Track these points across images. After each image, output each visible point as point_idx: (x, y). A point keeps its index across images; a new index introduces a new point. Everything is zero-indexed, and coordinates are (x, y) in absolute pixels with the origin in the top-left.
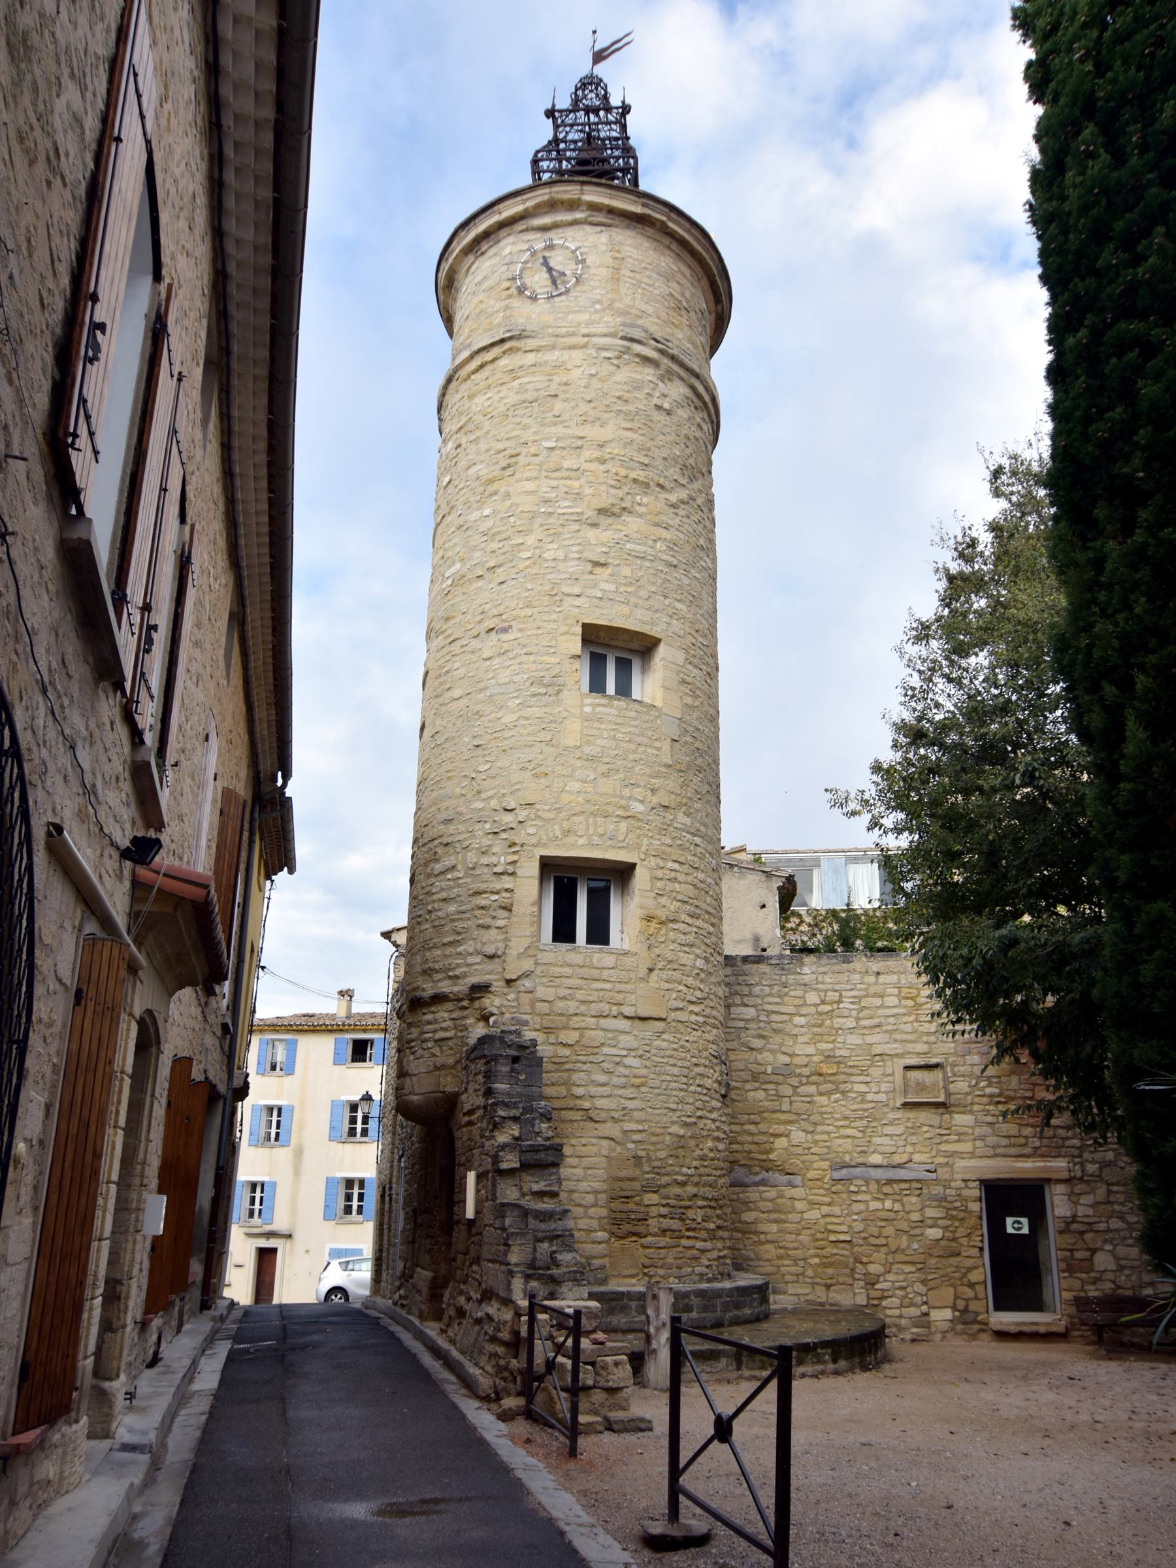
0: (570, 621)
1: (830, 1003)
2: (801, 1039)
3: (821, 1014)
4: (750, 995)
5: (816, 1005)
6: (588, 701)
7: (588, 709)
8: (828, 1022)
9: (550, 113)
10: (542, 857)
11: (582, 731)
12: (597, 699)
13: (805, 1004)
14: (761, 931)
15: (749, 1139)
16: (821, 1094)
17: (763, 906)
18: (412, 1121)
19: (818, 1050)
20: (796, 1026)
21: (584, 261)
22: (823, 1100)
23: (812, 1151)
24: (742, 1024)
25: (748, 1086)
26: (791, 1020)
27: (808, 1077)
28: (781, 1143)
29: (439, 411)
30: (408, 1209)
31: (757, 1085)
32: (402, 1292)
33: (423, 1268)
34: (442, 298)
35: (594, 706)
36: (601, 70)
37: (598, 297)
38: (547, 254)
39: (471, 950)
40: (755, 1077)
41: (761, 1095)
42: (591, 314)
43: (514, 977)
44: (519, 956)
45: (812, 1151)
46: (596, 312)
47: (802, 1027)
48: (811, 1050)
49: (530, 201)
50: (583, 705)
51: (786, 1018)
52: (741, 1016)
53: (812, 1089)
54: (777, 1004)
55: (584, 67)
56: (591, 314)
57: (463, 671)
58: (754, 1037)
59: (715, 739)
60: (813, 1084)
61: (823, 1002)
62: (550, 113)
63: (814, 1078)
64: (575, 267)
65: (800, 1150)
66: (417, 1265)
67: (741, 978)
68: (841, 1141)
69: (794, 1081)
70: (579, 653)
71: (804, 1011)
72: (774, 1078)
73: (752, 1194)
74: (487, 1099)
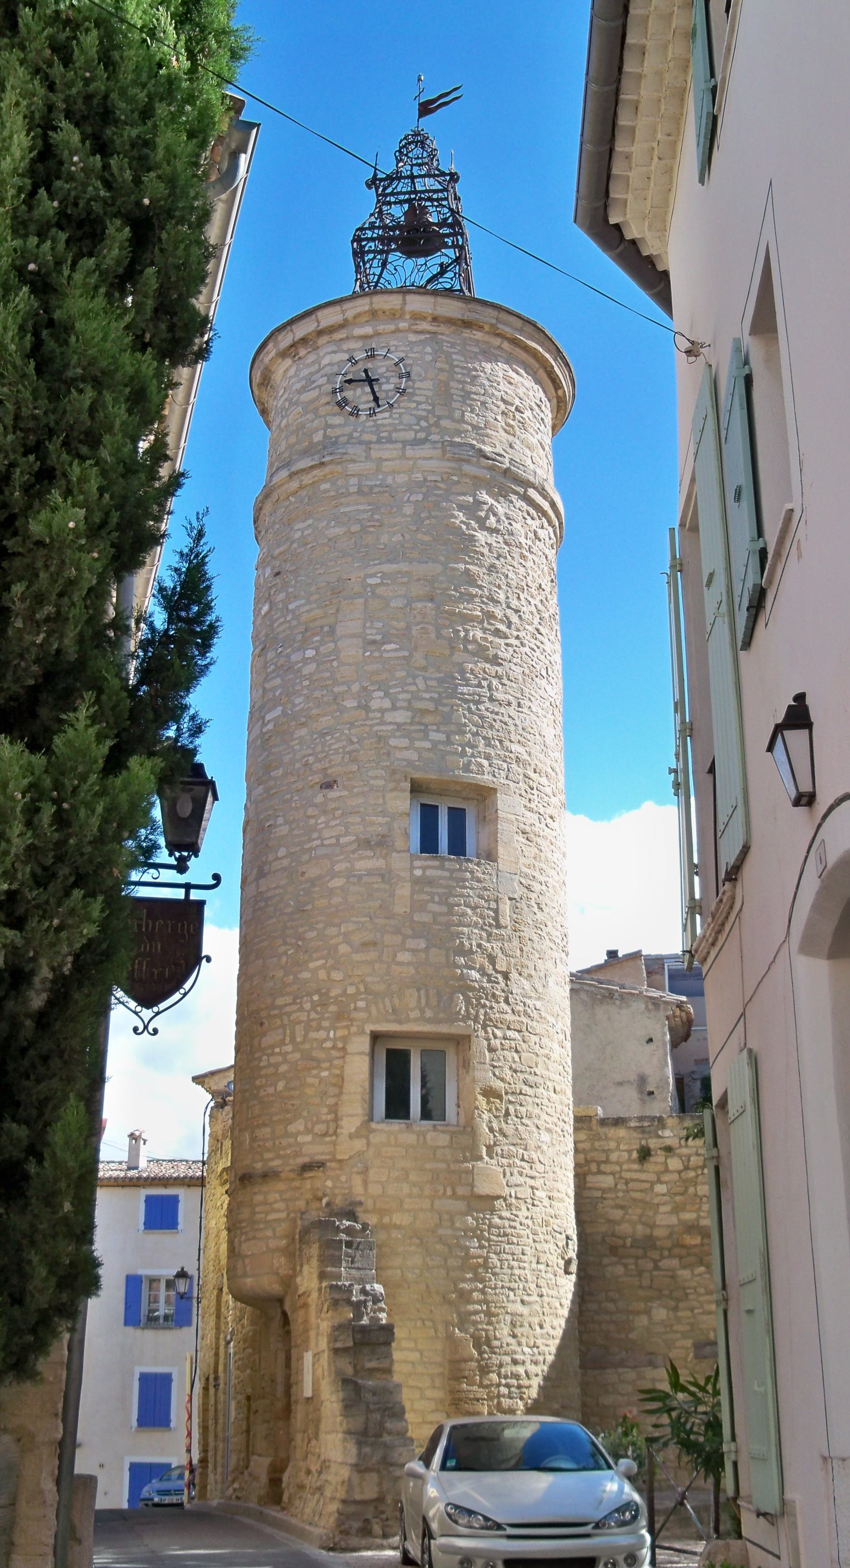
0: (398, 776)
1: (695, 1169)
2: (663, 1209)
3: (685, 1181)
4: (607, 1161)
5: (680, 1172)
6: (417, 863)
7: (418, 873)
8: (691, 1190)
9: (373, 183)
10: (372, 1032)
11: (412, 896)
12: (425, 860)
13: (667, 1170)
14: (648, 1070)
15: (607, 1317)
16: (684, 1267)
17: (650, 1040)
18: (242, 1302)
19: (679, 1220)
20: (658, 1195)
21: (408, 375)
22: (685, 1273)
23: (675, 1328)
24: (598, 1194)
25: (606, 1261)
26: (652, 1188)
27: (670, 1250)
28: (643, 1320)
29: (255, 522)
30: (239, 1397)
31: (614, 1259)
32: (236, 1485)
33: (259, 1455)
34: (256, 392)
35: (424, 868)
36: (428, 124)
37: (424, 414)
38: (369, 365)
39: (302, 1128)
40: (613, 1250)
41: (620, 1270)
42: (417, 432)
43: (346, 1157)
44: (351, 1136)
45: (675, 1328)
46: (422, 429)
47: (663, 1195)
48: (673, 1220)
49: (352, 309)
50: (412, 868)
51: (647, 1185)
52: (597, 1185)
53: (675, 1262)
54: (636, 1171)
55: (410, 122)
56: (417, 432)
57: (286, 862)
58: (612, 1207)
59: (708, 675)
60: (675, 1256)
61: (687, 1168)
62: (373, 183)
63: (676, 1251)
64: (397, 380)
65: (661, 1329)
66: (253, 1454)
67: (597, 1144)
68: (705, 1317)
69: (655, 1255)
70: (408, 811)
71: (666, 1178)
72: (633, 1251)
73: (611, 1375)
74: (321, 1282)
